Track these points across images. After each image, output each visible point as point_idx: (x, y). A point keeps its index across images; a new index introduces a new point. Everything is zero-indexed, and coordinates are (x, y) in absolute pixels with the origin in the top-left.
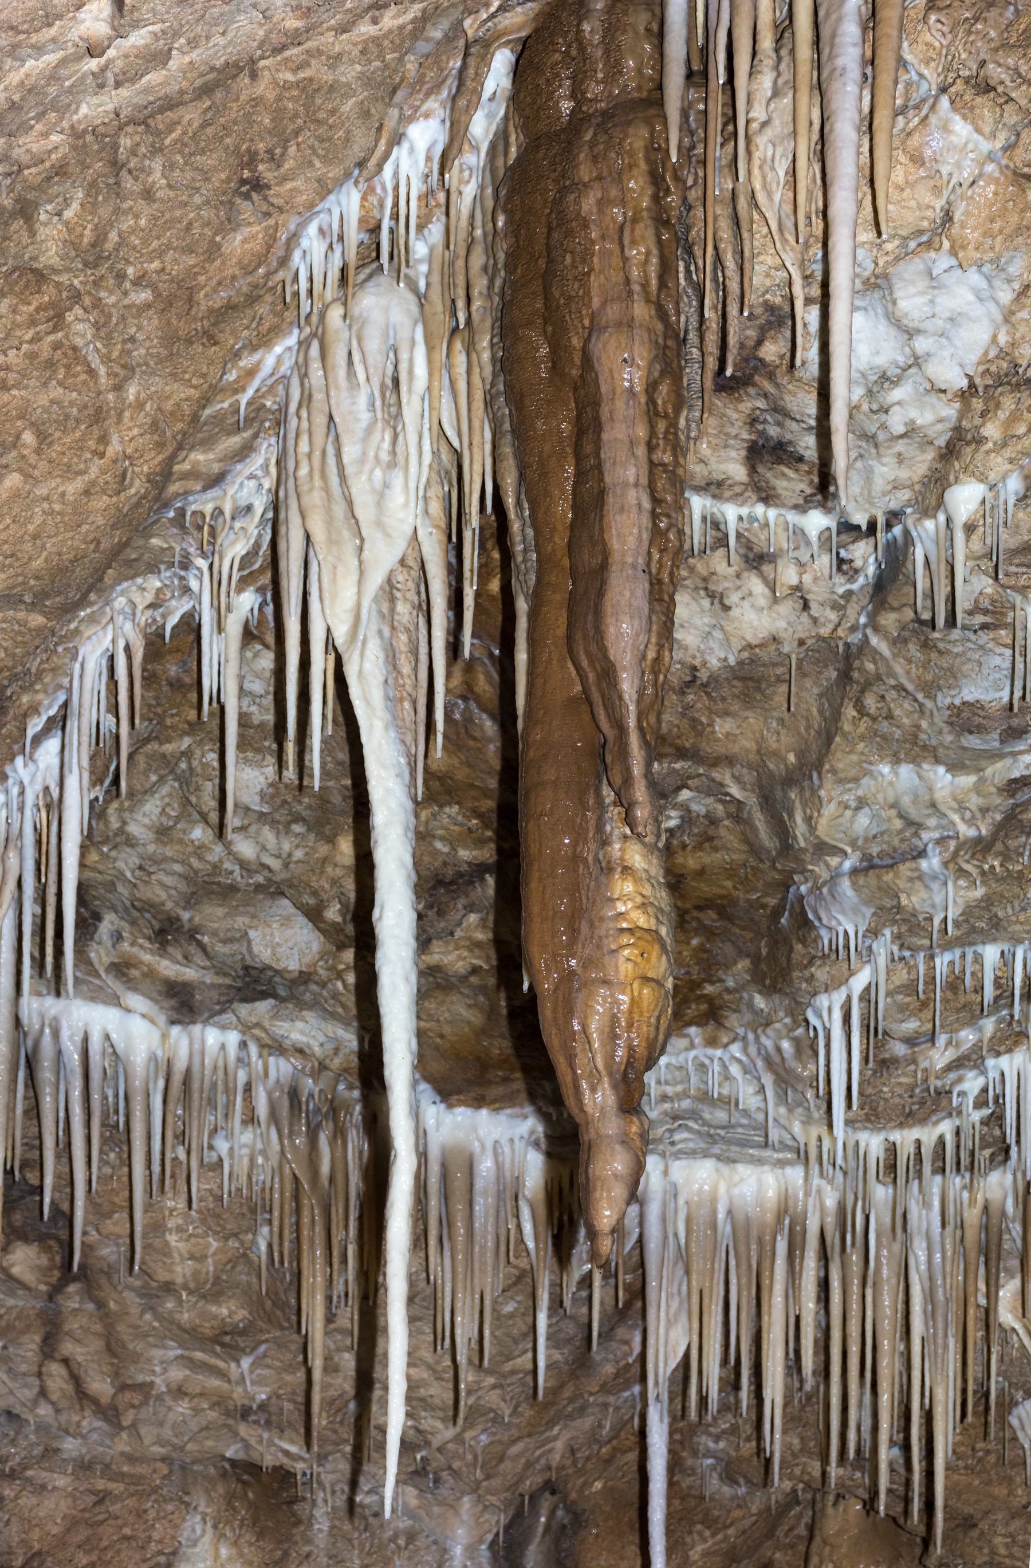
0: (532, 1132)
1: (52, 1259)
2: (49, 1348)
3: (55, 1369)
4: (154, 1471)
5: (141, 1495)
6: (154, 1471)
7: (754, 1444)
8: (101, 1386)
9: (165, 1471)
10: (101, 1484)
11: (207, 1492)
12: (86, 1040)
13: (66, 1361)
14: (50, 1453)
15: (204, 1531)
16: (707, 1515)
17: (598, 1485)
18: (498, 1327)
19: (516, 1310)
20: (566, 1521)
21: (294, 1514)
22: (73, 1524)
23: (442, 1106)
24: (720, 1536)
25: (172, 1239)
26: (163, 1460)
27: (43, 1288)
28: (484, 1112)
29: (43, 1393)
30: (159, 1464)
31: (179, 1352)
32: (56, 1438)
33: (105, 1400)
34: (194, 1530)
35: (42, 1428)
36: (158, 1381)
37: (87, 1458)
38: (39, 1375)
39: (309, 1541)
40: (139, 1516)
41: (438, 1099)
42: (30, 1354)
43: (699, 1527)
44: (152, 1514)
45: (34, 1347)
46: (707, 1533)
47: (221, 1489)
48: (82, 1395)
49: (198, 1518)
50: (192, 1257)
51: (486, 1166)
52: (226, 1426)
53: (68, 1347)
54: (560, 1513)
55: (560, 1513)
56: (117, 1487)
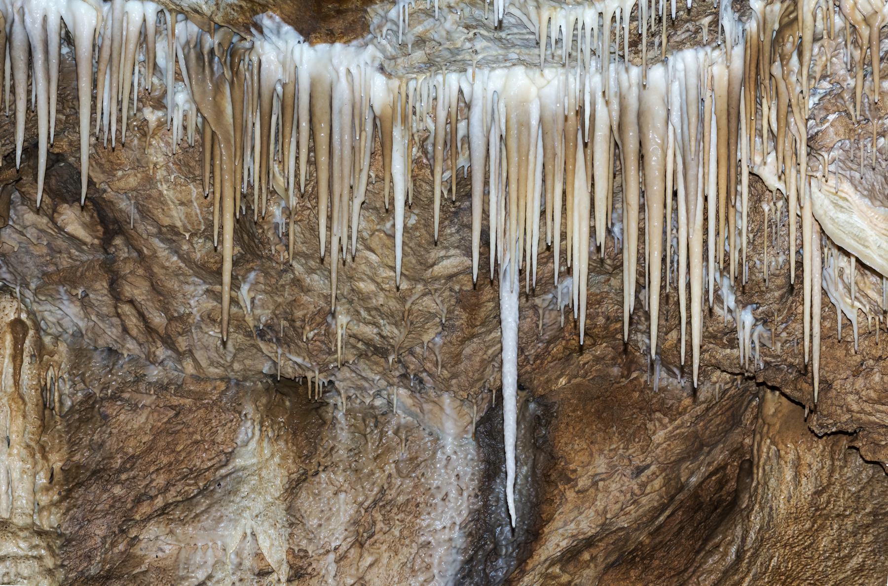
0: (374, 59)
1: (92, 217)
2: (116, 295)
3: (126, 309)
4: (215, 388)
5: (208, 408)
6: (215, 388)
7: (461, 277)
8: (158, 319)
9: (223, 388)
10: (175, 401)
11: (255, 402)
12: (45, 19)
13: (131, 302)
14: (139, 379)
15: (253, 434)
16: (663, 403)
17: (563, 381)
18: (411, 239)
19: (418, 222)
20: (539, 413)
21: (321, 418)
22: (157, 434)
23: (306, 45)
24: (678, 422)
25: (163, 188)
26: (222, 379)
27: (96, 241)
28: (338, 46)
29: (125, 330)
30: (218, 383)
31: (204, 287)
32: (143, 367)
33: (162, 331)
34: (247, 433)
35: (133, 359)
36: (195, 311)
37: (166, 381)
38: (118, 315)
39: (334, 438)
40: (206, 424)
41: (302, 38)
42: (105, 298)
43: (658, 415)
44: (214, 423)
45: (106, 292)
46: (666, 420)
47: (264, 400)
48: (150, 329)
49: (249, 423)
50: (182, 204)
51: (342, 91)
52: (253, 345)
53: (128, 291)
54: (532, 406)
55: (532, 406)
56: (188, 402)
